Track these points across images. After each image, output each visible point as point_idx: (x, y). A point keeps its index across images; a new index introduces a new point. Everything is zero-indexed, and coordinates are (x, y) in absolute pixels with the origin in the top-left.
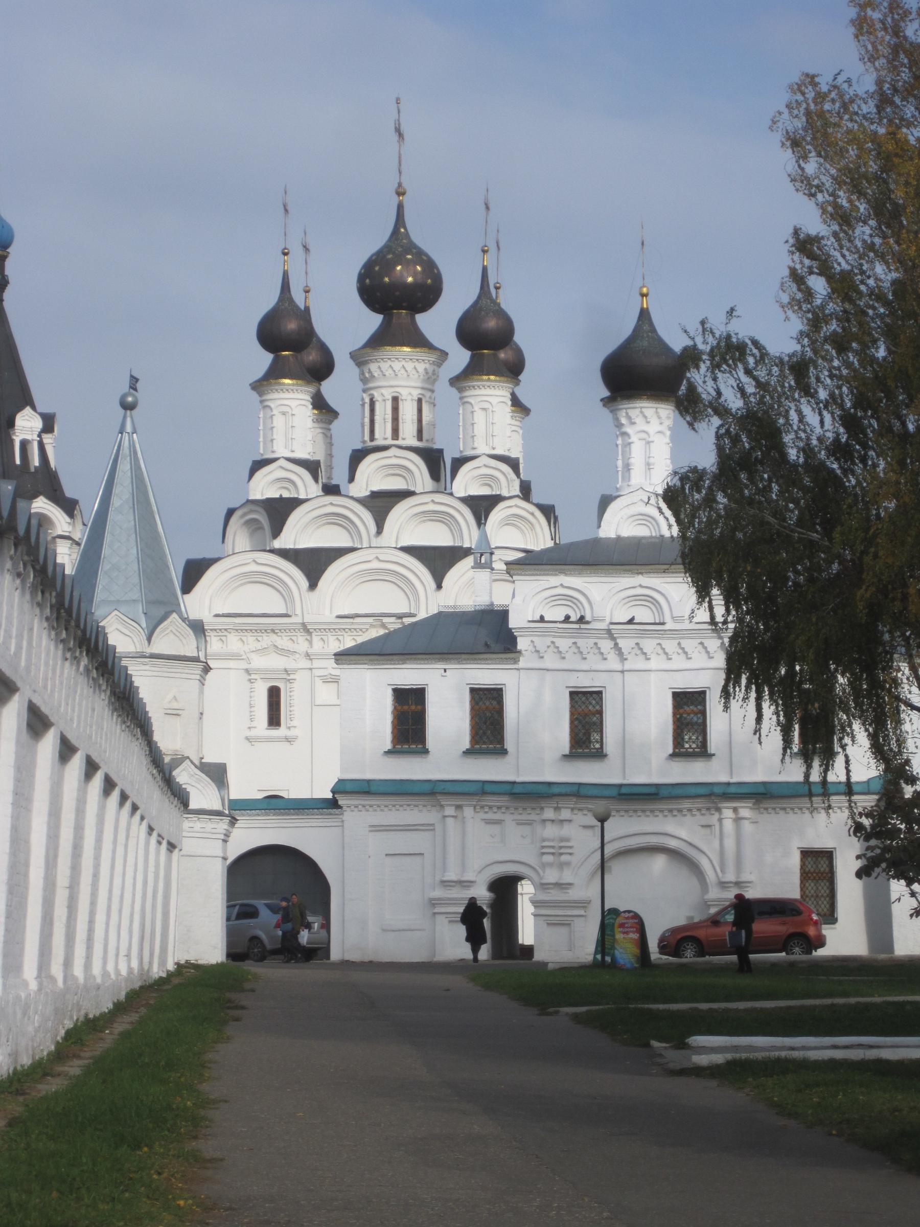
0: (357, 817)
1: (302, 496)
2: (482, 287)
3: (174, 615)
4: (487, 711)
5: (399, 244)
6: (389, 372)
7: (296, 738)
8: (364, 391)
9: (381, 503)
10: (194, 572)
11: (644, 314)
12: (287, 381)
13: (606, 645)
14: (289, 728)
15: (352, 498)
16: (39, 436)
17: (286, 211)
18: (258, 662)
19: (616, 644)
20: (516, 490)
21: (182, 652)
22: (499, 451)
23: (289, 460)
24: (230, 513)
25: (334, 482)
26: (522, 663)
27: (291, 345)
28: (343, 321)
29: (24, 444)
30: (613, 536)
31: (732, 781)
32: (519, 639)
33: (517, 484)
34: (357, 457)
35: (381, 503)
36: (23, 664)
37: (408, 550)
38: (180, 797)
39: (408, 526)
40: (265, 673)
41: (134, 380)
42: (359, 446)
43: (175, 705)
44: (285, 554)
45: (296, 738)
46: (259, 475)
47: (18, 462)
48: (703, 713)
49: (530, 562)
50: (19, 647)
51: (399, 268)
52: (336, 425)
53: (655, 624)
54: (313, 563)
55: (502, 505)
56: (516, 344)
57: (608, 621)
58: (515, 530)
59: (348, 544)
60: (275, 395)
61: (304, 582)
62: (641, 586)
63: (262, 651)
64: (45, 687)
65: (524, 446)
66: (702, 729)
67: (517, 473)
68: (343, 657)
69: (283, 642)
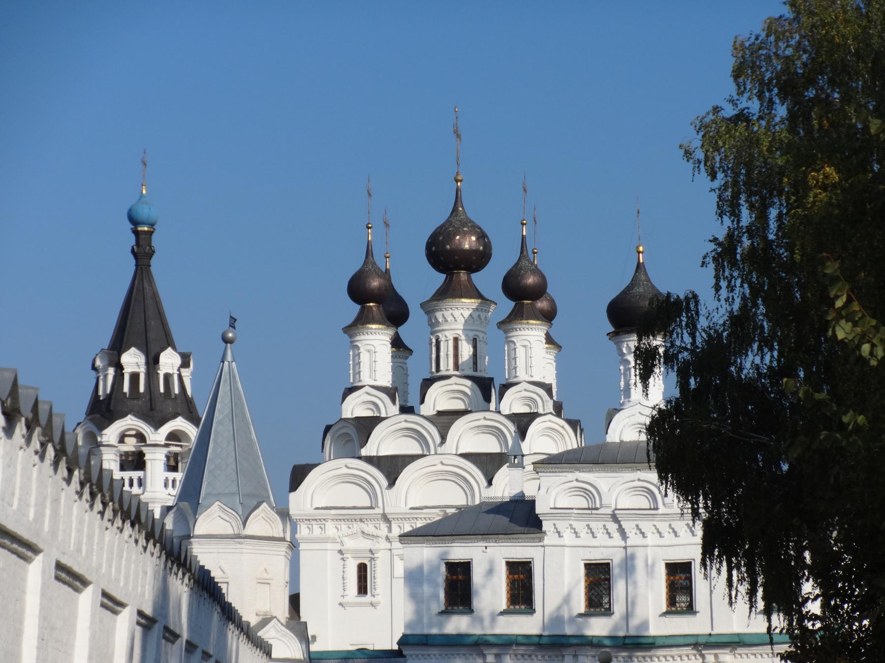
1: (383, 415)
2: (522, 252)
3: (265, 504)
5: (456, 222)
6: (450, 318)
7: (378, 603)
8: (432, 333)
9: (445, 420)
10: (298, 475)
11: (639, 266)
12: (374, 326)
13: (613, 527)
14: (374, 596)
15: (423, 416)
16: (179, 370)
17: (370, 194)
18: (350, 544)
19: (620, 526)
20: (550, 407)
21: (270, 534)
22: (536, 379)
23: (372, 387)
24: (328, 428)
25: (409, 404)
26: (547, 541)
27: (376, 300)
28: (416, 280)
29: (168, 377)
30: (618, 441)
31: (712, 633)
32: (544, 523)
33: (551, 403)
34: (427, 383)
35: (445, 420)
36: (46, 527)
37: (465, 456)
39: (469, 436)
40: (356, 552)
41: (233, 320)
42: (428, 376)
43: (265, 576)
44: (369, 460)
45: (378, 603)
46: (349, 398)
47: (162, 390)
48: (690, 579)
49: (552, 462)
50: (40, 515)
51: (458, 237)
52: (411, 361)
53: (650, 509)
54: (392, 467)
55: (538, 420)
56: (549, 295)
57: (613, 507)
58: (548, 437)
59: (419, 452)
60: (362, 337)
61: (384, 482)
62: (639, 480)
63: (352, 535)
64: (79, 550)
65: (557, 375)
66: (688, 589)
67: (551, 396)
68: (405, 537)
69: (369, 528)
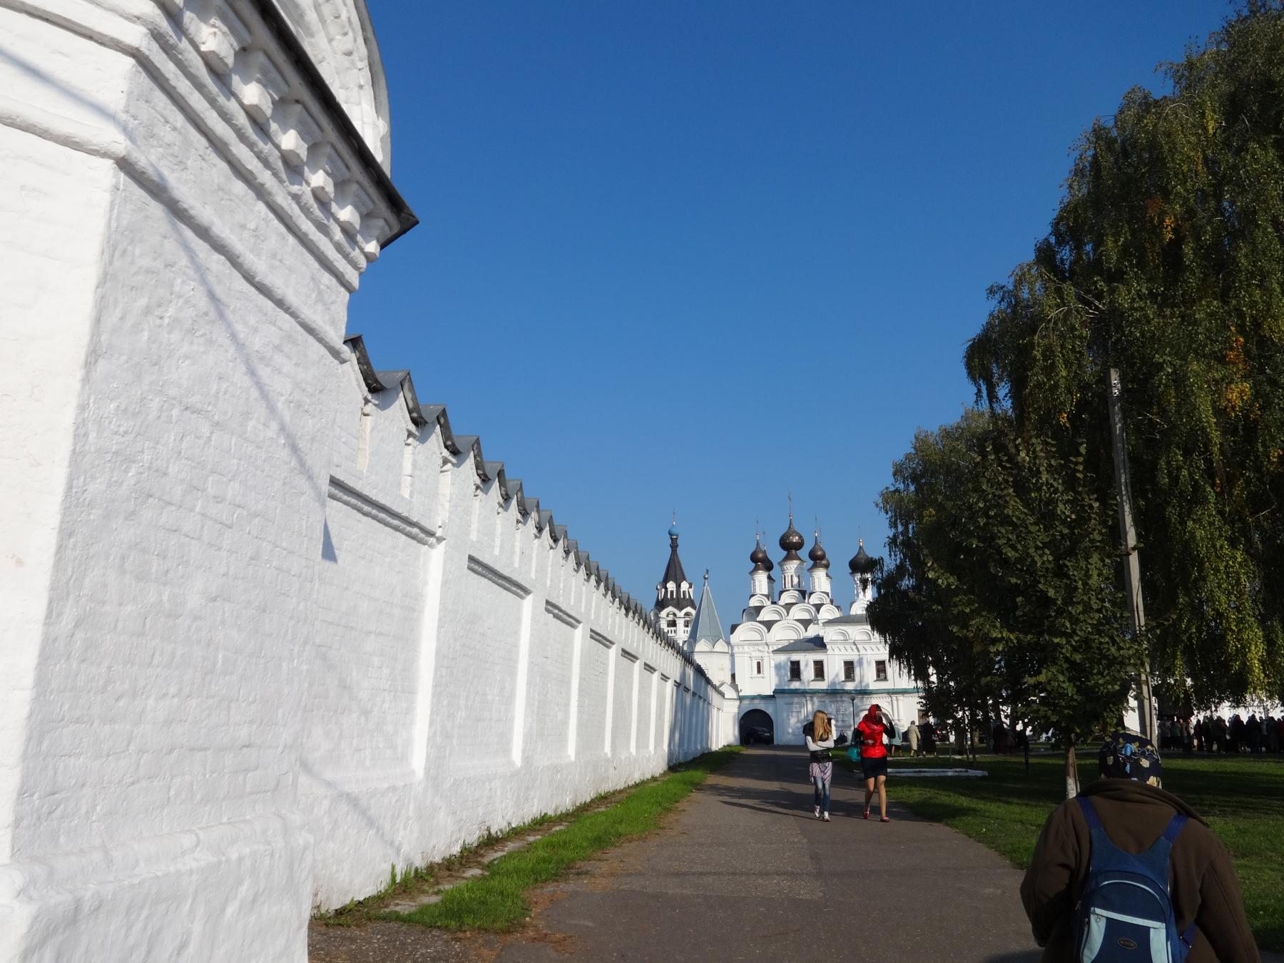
0: (781, 700)
4: (819, 666)
9: (788, 607)
10: (734, 628)
18: (754, 654)
27: (761, 562)
28: (776, 554)
34: (781, 593)
35: (788, 607)
38: (722, 695)
54: (769, 625)
